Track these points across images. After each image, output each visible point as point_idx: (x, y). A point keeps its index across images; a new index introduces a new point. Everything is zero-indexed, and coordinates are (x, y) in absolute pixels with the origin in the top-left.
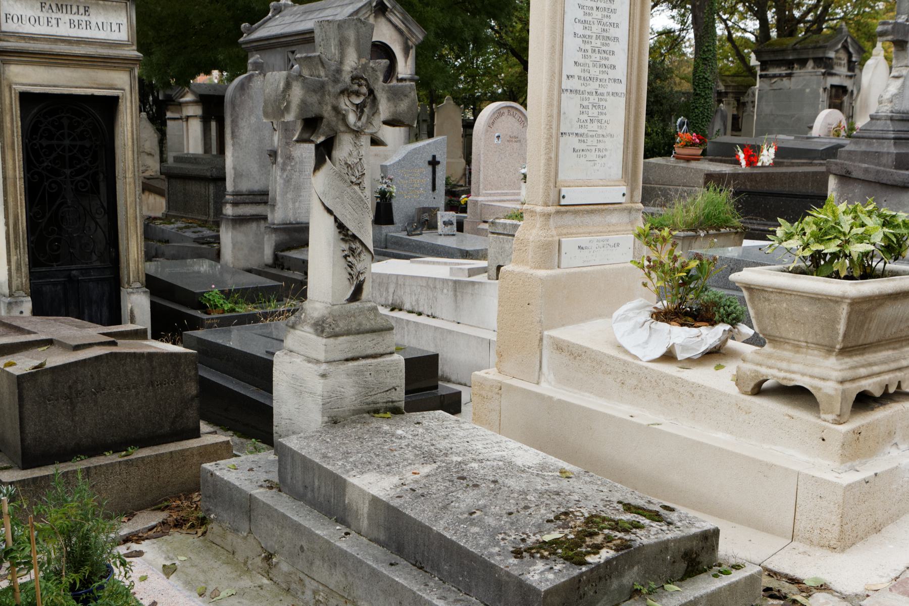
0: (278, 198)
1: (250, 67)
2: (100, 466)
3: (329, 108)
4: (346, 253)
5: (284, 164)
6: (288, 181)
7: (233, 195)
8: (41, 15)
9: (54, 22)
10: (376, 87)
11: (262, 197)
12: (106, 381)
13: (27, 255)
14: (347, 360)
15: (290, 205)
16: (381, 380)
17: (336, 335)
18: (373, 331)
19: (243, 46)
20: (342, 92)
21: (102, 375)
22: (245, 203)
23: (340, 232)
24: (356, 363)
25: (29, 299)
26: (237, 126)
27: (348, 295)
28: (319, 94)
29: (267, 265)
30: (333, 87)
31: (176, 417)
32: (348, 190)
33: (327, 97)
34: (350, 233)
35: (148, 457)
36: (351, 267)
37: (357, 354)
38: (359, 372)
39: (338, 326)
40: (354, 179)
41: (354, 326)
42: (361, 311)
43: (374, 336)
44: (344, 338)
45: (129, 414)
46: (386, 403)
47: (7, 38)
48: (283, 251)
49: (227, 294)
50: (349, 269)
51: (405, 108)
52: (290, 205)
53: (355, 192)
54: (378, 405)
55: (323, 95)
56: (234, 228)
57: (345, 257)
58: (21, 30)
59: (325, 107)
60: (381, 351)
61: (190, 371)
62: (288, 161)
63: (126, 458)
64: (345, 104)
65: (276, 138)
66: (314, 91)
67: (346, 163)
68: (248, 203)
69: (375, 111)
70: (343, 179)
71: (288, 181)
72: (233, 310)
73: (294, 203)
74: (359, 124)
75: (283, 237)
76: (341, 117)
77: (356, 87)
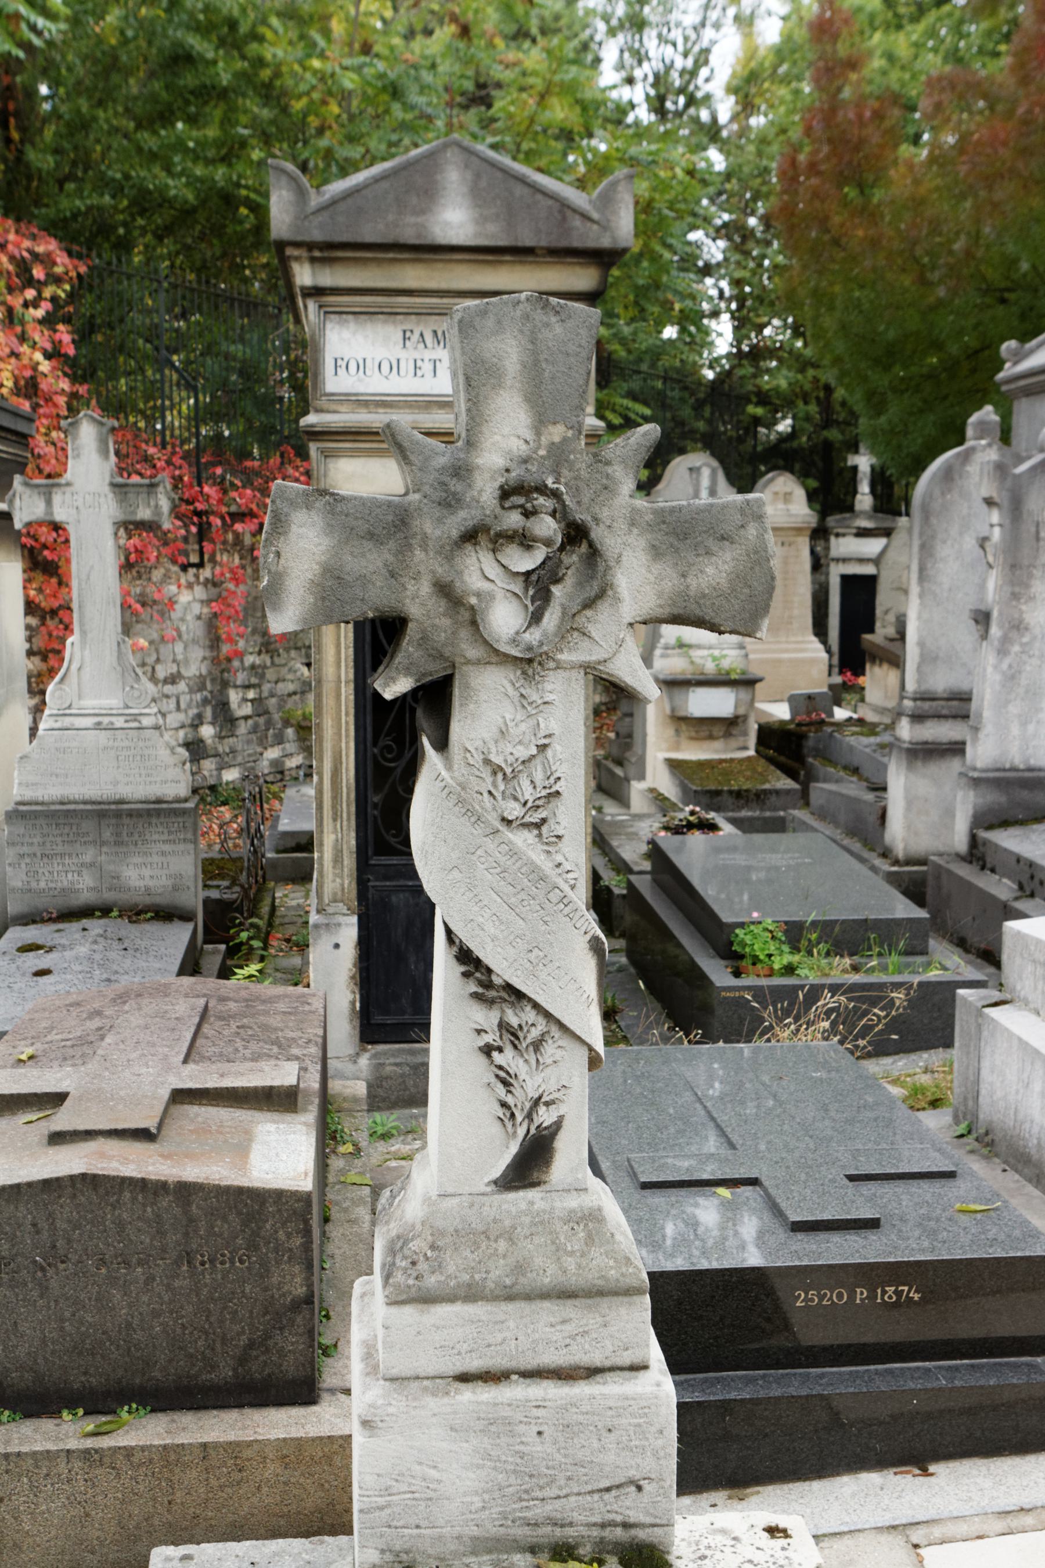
0: (986, 714)
1: (970, 432)
2: (19, 1454)
3: (425, 588)
4: (488, 1038)
5: (1005, 640)
6: (1011, 678)
7: (915, 699)
8: (403, 355)
9: (427, 367)
10: (605, 514)
11: (958, 705)
12: (69, 1241)
13: (353, 834)
14: (464, 1378)
15: (1015, 730)
16: (580, 1455)
17: (427, 1299)
18: (566, 1294)
19: (1004, 388)
20: (470, 536)
21: (61, 1225)
22: (939, 717)
23: (466, 975)
25: (354, 919)
26: (931, 555)
27: (498, 1170)
28: (392, 545)
29: (958, 855)
30: (440, 521)
31: (251, 1345)
32: (490, 844)
33: (418, 553)
34: (497, 981)
35: (143, 1448)
36: (505, 1083)
38: (494, 1425)
39: (438, 1267)
40: (514, 810)
41: (498, 1272)
42: (541, 1222)
43: (568, 1309)
44: (458, 1308)
45: (129, 1325)
46: (603, 1526)
47: (333, 407)
48: (990, 827)
49: (794, 934)
50: (501, 1090)
51: (723, 580)
52: (1015, 730)
53: (514, 853)
54: (570, 1531)
55: (405, 549)
56: (910, 767)
57: (487, 1050)
58: (361, 389)
59: (411, 587)
60: (597, 1359)
61: (289, 1236)
62: (1014, 634)
63: (90, 1443)
64: (483, 573)
65: (991, 585)
66: (371, 536)
67: (487, 762)
68: (945, 717)
69: (597, 594)
70: (469, 812)
71: (1013, 677)
72: (790, 970)
73: (1024, 724)
74: (533, 636)
75: (992, 797)
76: (467, 615)
77: (514, 520)
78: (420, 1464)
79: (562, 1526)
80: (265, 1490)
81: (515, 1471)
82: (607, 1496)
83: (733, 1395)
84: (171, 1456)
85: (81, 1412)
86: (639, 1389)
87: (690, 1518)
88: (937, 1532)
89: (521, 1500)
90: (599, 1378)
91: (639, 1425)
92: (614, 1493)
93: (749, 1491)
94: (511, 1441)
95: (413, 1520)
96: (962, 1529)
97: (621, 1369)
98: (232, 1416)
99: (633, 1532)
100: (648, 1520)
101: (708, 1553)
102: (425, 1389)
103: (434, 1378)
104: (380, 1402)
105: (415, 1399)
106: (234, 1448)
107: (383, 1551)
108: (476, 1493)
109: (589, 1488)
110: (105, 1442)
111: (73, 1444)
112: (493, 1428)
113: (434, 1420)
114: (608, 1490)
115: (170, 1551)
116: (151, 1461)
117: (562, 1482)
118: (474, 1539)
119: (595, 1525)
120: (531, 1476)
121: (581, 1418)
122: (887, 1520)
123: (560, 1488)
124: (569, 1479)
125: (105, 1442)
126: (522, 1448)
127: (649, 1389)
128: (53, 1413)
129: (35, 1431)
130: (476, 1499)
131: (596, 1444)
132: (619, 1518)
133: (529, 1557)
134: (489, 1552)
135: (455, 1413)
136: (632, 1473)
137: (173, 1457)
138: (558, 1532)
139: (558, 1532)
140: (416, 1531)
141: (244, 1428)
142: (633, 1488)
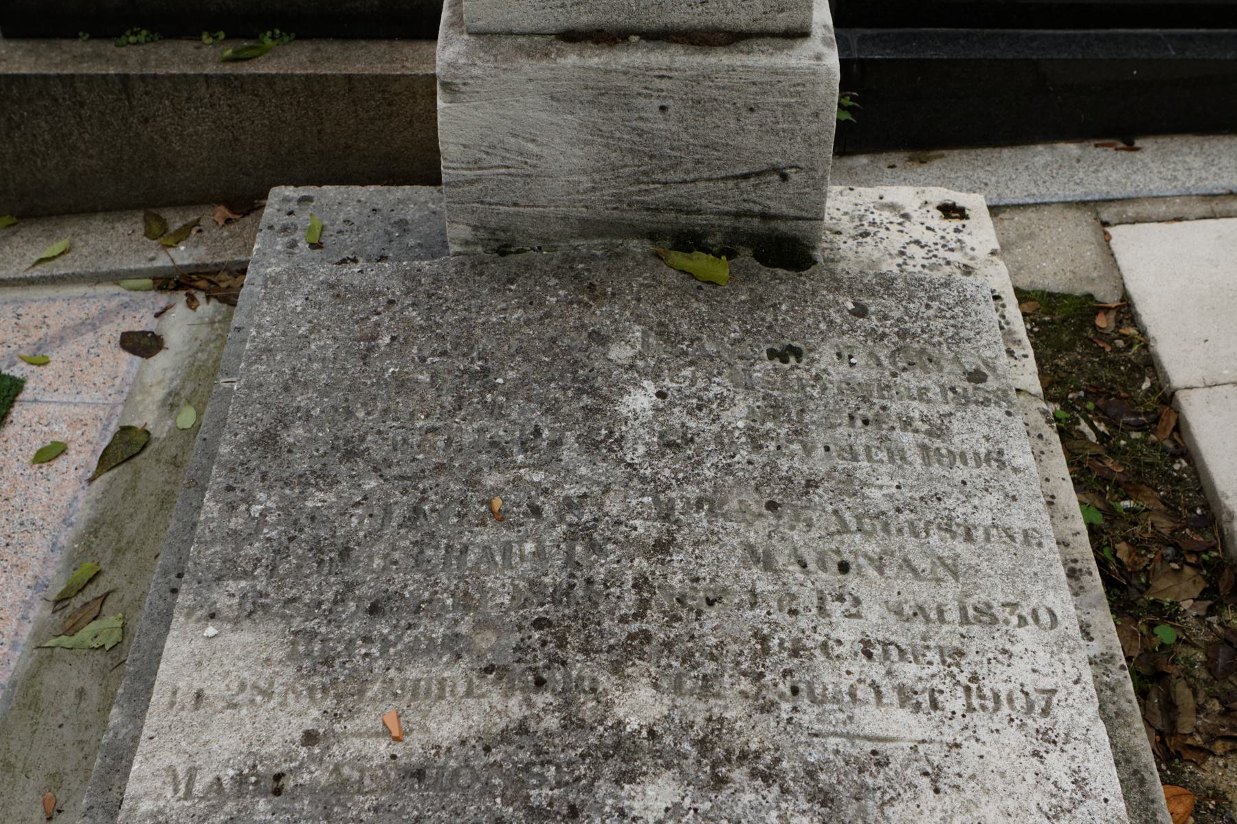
2: (155, 76)
14: (571, 36)
16: (712, 136)
24: (596, 59)
35: (285, 77)
37: (620, 19)
38: (603, 95)
46: (737, 215)
54: (699, 219)
60: (741, 19)
63: (228, 69)
78: (515, 136)
79: (688, 213)
80: (417, 125)
81: (631, 150)
82: (743, 184)
83: (929, 54)
84: (313, 87)
85: (222, 35)
86: (793, 62)
87: (858, 189)
88: (1131, 211)
89: (639, 182)
90: (742, 46)
91: (789, 105)
92: (752, 181)
93: (932, 153)
94: (628, 115)
95: (510, 197)
96: (1162, 209)
97: (773, 35)
98: (381, 47)
99: (773, 224)
100: (792, 212)
101: (872, 229)
102: (520, 48)
103: (531, 34)
104: (462, 61)
105: (506, 60)
106: (381, 81)
107: (475, 228)
108: (585, 172)
109: (723, 174)
110: (246, 69)
111: (210, 69)
112: (604, 100)
113: (530, 86)
114: (746, 177)
115: (290, 191)
116: (294, 90)
117: (690, 166)
118: (583, 221)
119: (728, 213)
120: (652, 157)
121: (715, 93)
122: (1078, 193)
123: (687, 172)
124: (698, 162)
125: (246, 69)
126: (641, 124)
127: (806, 63)
128: (195, 36)
129: (174, 53)
130: (584, 178)
131: (733, 125)
132: (757, 208)
133: (648, 245)
134: (601, 235)
135: (556, 79)
136: (776, 159)
137: (317, 88)
138: (683, 218)
139: (683, 218)
140: (513, 209)
141: (392, 61)
142: (777, 177)
